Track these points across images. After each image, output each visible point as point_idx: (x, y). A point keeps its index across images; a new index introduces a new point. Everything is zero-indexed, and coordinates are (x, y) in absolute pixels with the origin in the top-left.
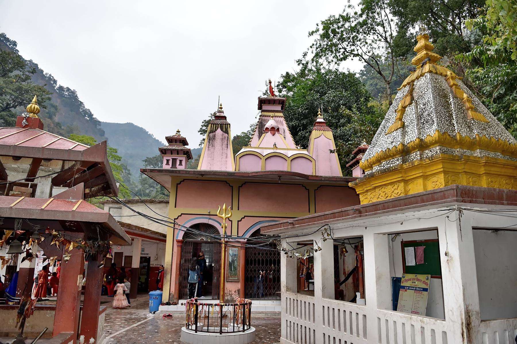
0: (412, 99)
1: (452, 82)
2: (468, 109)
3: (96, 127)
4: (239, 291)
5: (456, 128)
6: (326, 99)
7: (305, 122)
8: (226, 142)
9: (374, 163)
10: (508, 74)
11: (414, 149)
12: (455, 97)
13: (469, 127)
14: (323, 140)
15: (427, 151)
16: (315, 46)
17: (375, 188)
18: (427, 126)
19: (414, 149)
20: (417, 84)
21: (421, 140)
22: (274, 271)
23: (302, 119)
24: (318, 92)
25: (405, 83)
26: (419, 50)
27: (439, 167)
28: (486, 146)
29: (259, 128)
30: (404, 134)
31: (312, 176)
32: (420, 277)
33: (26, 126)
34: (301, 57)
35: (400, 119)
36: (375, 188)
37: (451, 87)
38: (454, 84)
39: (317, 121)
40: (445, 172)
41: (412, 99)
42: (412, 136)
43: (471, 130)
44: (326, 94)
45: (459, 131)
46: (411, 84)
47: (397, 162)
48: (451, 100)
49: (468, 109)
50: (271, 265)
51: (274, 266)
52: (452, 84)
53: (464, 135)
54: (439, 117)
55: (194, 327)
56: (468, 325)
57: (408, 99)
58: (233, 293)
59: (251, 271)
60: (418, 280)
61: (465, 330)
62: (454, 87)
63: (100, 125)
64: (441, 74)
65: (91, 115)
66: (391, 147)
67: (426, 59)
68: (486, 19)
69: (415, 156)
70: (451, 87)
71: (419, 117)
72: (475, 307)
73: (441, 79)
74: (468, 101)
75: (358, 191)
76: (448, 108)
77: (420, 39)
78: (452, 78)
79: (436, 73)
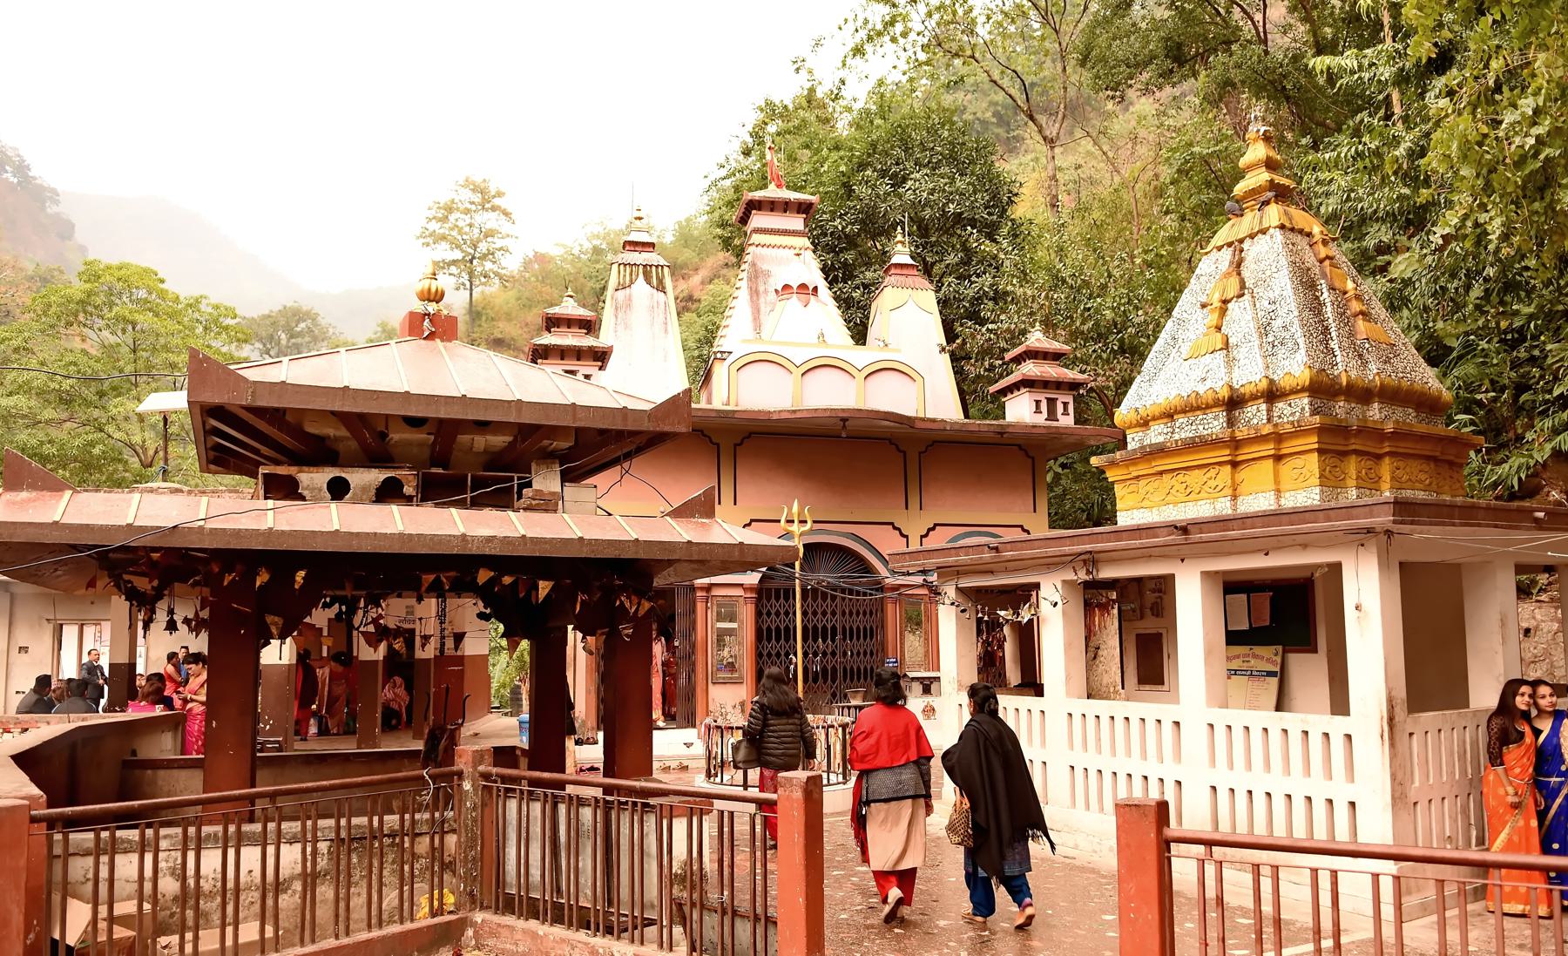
0: (1243, 285)
1: (1323, 252)
2: (1356, 315)
3: (43, 208)
4: (742, 704)
5: (1339, 359)
6: (909, 195)
7: (849, 256)
8: (662, 316)
9: (1154, 419)
10: (1401, 198)
11: (1254, 397)
12: (1332, 288)
13: (1360, 356)
14: (909, 315)
15: (1280, 405)
16: (851, 26)
17: (1161, 473)
18: (1281, 351)
19: (1254, 397)
20: (1252, 250)
21: (1272, 382)
22: (824, 654)
23: (841, 250)
24: (883, 174)
25: (1219, 239)
26: (1250, 167)
27: (1312, 441)
28: (1391, 395)
29: (750, 279)
30: (1230, 362)
31: (923, 420)
32: (1258, 650)
33: (431, 336)
34: (804, 51)
35: (1219, 328)
36: (1161, 473)
37: (1321, 261)
38: (1327, 257)
39: (894, 261)
40: (1320, 451)
41: (1243, 285)
42: (1249, 373)
43: (1365, 364)
44: (904, 180)
45: (1344, 368)
46: (1237, 246)
47: (1215, 424)
48: (1326, 295)
49: (1356, 315)
50: (815, 640)
51: (824, 641)
52: (1323, 255)
53: (1353, 374)
54: (1308, 335)
55: (718, 780)
56: (1391, 719)
57: (1233, 284)
58: (729, 709)
59: (769, 655)
60: (1255, 656)
61: (1386, 728)
62: (1327, 262)
63: (57, 203)
64: (1301, 232)
65: (22, 169)
66: (1201, 389)
67: (1270, 194)
68: (1366, 62)
69: (1255, 414)
70: (1321, 261)
71: (1264, 330)
72: (1401, 693)
73: (1302, 242)
74: (1358, 297)
75: (1111, 475)
76: (1320, 313)
77: (1255, 140)
78: (1325, 243)
79: (1292, 230)
